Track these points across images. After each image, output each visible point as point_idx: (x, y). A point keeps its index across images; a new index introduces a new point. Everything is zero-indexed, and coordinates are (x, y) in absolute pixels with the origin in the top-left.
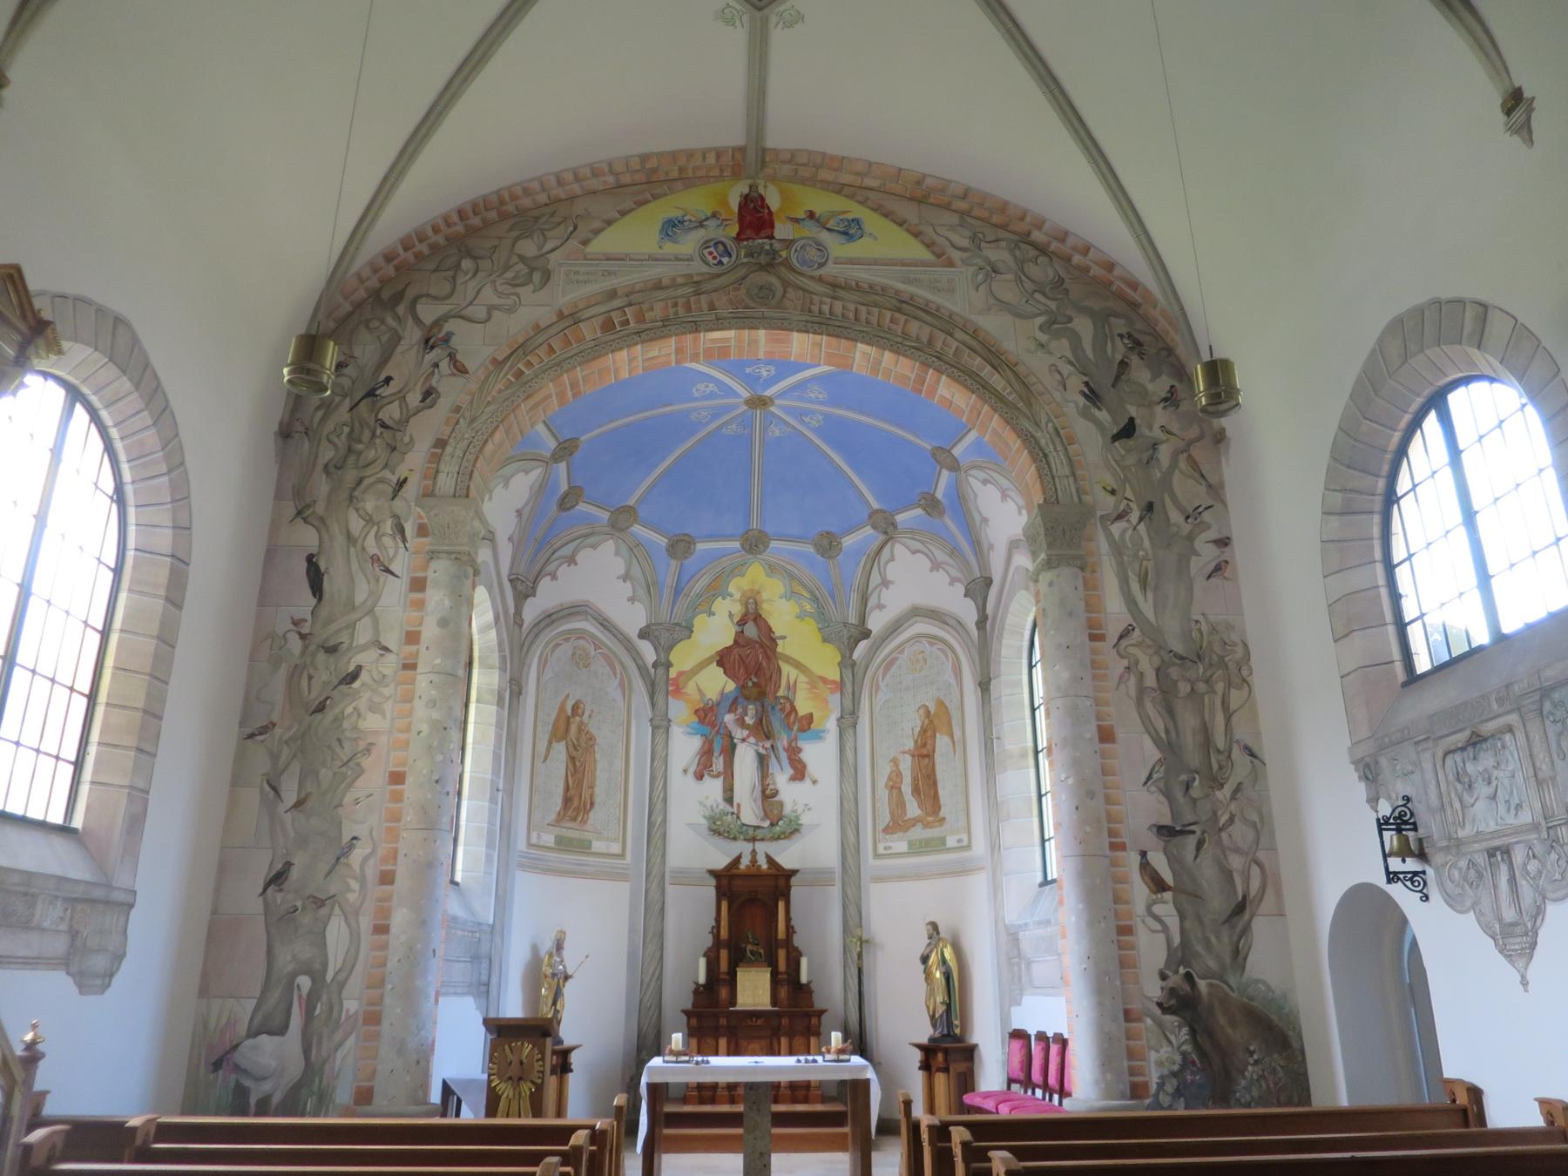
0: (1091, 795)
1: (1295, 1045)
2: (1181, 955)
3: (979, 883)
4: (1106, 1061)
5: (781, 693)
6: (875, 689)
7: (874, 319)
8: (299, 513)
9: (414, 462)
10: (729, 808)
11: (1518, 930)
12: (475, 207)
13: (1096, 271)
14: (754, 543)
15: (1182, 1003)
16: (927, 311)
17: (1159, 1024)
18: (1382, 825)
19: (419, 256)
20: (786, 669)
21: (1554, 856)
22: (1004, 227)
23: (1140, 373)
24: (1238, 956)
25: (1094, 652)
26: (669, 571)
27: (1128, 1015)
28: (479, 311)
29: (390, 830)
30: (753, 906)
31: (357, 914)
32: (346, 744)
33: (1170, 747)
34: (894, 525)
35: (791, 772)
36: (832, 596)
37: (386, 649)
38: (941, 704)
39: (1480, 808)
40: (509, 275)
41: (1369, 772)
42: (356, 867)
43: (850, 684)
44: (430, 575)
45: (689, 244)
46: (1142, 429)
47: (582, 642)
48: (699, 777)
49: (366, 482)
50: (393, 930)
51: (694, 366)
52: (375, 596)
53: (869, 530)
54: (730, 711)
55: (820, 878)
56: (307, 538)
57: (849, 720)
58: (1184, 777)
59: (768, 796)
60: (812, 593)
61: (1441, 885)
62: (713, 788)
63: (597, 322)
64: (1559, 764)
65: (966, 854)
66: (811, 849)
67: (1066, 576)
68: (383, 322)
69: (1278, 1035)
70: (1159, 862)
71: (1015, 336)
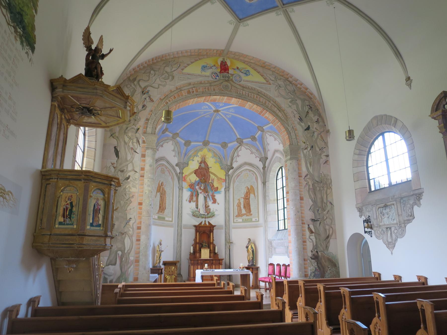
0: (298, 212)
1: (338, 266)
2: (315, 247)
3: (261, 230)
4: (300, 270)
5: (210, 181)
6: (234, 182)
7: (252, 96)
8: (111, 135)
9: (141, 124)
10: (197, 210)
11: (391, 243)
12: (156, 58)
13: (303, 89)
14: (206, 144)
15: (315, 257)
16: (265, 96)
17: (311, 262)
18: (364, 221)
19: (140, 69)
20: (211, 175)
21: (400, 229)
22: (282, 76)
23: (311, 115)
24: (327, 247)
25: (299, 180)
26: (184, 149)
27: (305, 260)
28: (156, 85)
29: (139, 216)
30: (205, 234)
31: (132, 236)
32: (127, 195)
33: (314, 202)
34: (243, 142)
35: (213, 201)
36: (224, 158)
37: (136, 172)
38: (252, 187)
39: (386, 219)
40: (163, 76)
41: (360, 210)
42: (131, 225)
43: (228, 180)
44: (146, 153)
45: (208, 73)
46: (311, 128)
47: (163, 167)
48: (190, 202)
49: (129, 128)
50: (141, 240)
51: (207, 103)
52: (133, 158)
53: (236, 143)
54: (197, 186)
55: (220, 227)
56: (114, 142)
57: (227, 189)
58: (317, 208)
59: (207, 207)
61: (375, 234)
62: (193, 204)
63: (186, 91)
64: (403, 212)
65: (258, 223)
66: (218, 220)
67: (294, 162)
68: (131, 86)
69: (334, 264)
70: (312, 227)
71: (284, 103)
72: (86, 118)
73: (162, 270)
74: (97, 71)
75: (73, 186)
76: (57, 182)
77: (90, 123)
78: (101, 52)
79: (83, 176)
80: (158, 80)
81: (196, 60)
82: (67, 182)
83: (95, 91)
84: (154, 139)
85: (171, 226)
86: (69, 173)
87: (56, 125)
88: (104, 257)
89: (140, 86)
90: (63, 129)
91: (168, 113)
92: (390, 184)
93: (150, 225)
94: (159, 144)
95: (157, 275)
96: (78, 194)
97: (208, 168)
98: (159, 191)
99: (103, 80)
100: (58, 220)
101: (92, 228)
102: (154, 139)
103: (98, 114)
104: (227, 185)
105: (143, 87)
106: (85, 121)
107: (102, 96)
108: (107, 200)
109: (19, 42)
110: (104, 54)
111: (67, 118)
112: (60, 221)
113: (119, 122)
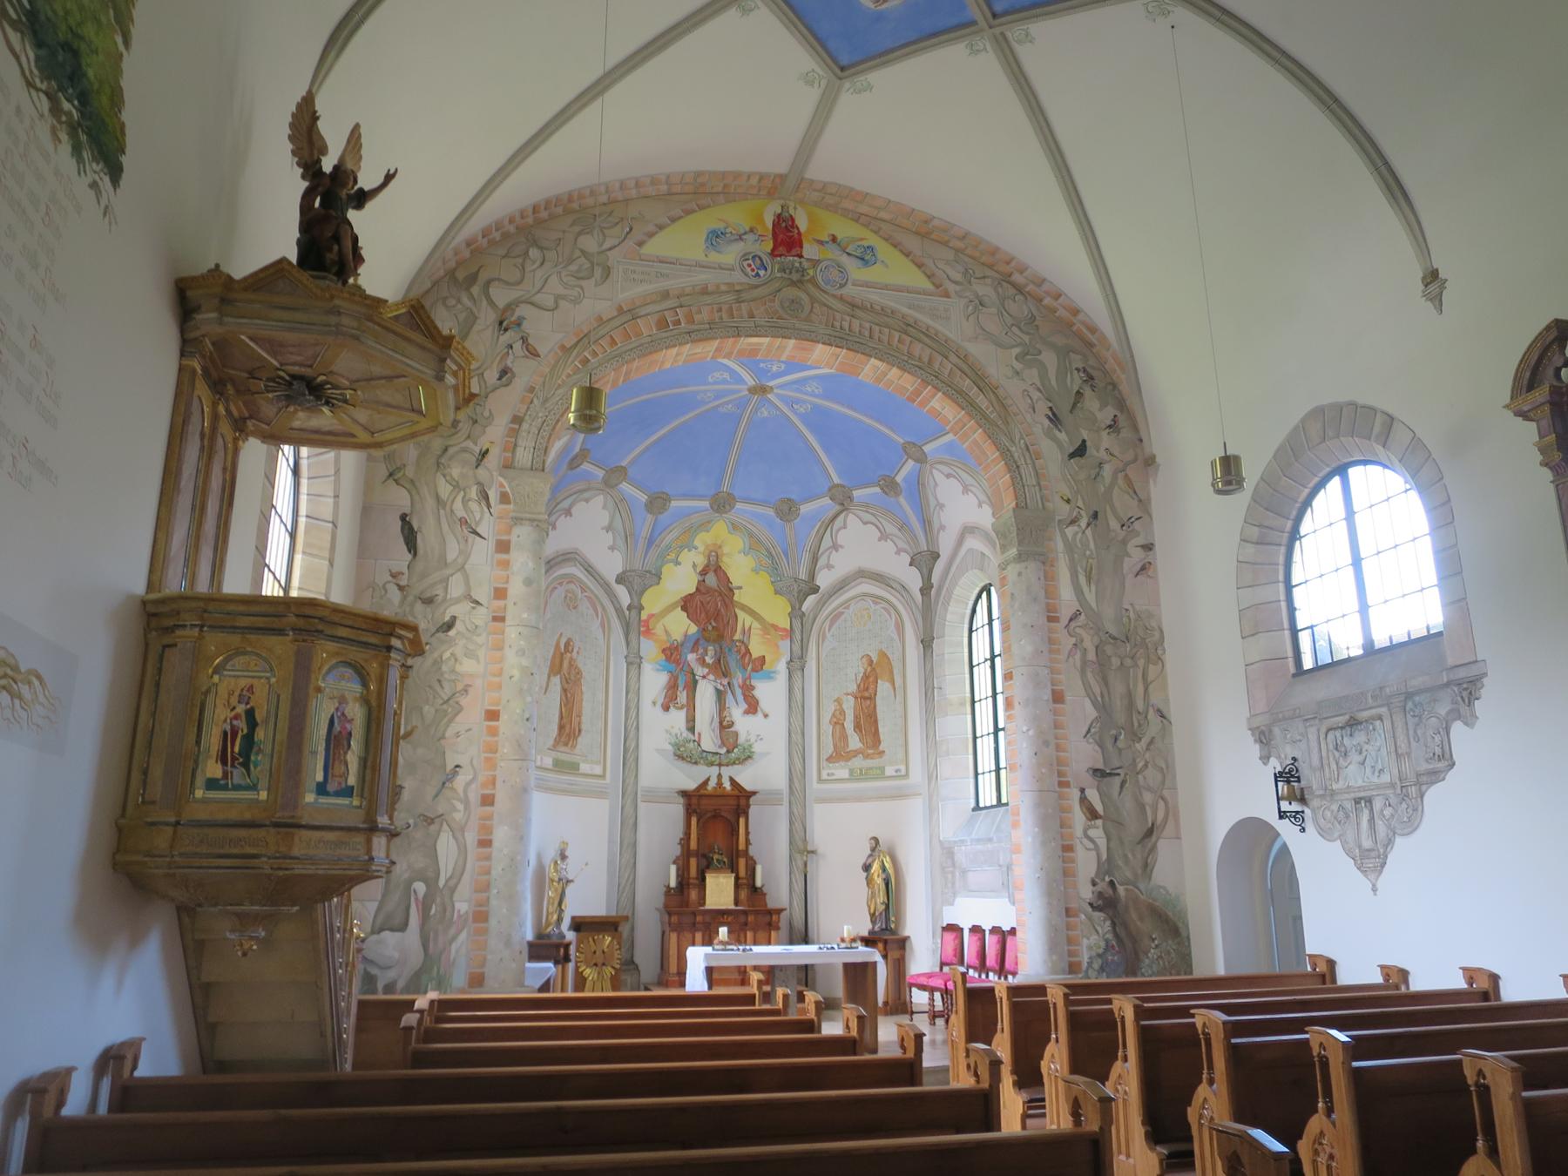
0: (1046, 743)
1: (1184, 934)
2: (1106, 867)
3: (917, 806)
4: (1053, 946)
5: (737, 637)
6: (822, 638)
7: (885, 338)
8: (391, 475)
9: (495, 434)
10: (691, 736)
11: (1373, 854)
12: (548, 203)
13: (1062, 313)
14: (722, 504)
15: (1107, 903)
16: (929, 336)
17: (1090, 918)
18: (1277, 777)
19: (492, 243)
20: (741, 615)
21: (1404, 805)
22: (991, 267)
23: (1091, 402)
24: (1147, 867)
25: (1051, 631)
26: (646, 523)
27: (1068, 912)
28: (546, 299)
29: (487, 759)
30: (717, 822)
31: (462, 830)
32: (445, 684)
33: (1103, 708)
34: (851, 498)
35: (746, 706)
36: (786, 555)
37: (477, 603)
38: (883, 655)
39: (1353, 769)
40: (573, 268)
41: (1264, 738)
42: (460, 790)
43: (799, 631)
44: (514, 538)
45: (730, 255)
46: (1091, 450)
47: (572, 586)
48: (666, 708)
49: (451, 451)
50: (496, 844)
51: (725, 361)
52: (466, 554)
53: (826, 501)
54: (692, 651)
55: (772, 798)
56: (400, 498)
57: (797, 664)
58: (1114, 732)
59: (725, 726)
60: (768, 550)
61: (1315, 820)
62: (678, 718)
63: (652, 320)
64: (1414, 744)
65: (904, 782)
66: (764, 772)
67: (1032, 569)
68: (459, 301)
69: (1172, 927)
70: (1093, 796)
71: (996, 363)
72: (301, 414)
73: (567, 946)
74: (340, 250)
75: (257, 655)
76: (200, 638)
77: (317, 432)
78: (355, 182)
79: (292, 619)
80: (554, 280)
81: (688, 212)
82: (235, 640)
83: (333, 319)
84: (540, 486)
85: (600, 794)
86: (242, 608)
87: (197, 437)
88: (365, 902)
89: (491, 303)
90: (222, 453)
91: (590, 397)
92: (1369, 646)
93: (525, 790)
94: (558, 506)
95: (550, 965)
96: (273, 680)
97: (731, 590)
98: (559, 672)
99: (362, 281)
100: (203, 771)
101: (323, 800)
102: (540, 486)
103: (346, 401)
104: (797, 648)
105: (501, 304)
106: (296, 424)
107: (357, 338)
108: (374, 703)
109: (66, 147)
110: (366, 189)
111: (236, 413)
112: (209, 775)
113: (416, 428)
